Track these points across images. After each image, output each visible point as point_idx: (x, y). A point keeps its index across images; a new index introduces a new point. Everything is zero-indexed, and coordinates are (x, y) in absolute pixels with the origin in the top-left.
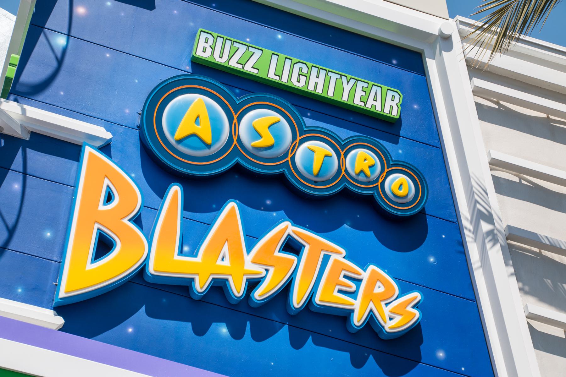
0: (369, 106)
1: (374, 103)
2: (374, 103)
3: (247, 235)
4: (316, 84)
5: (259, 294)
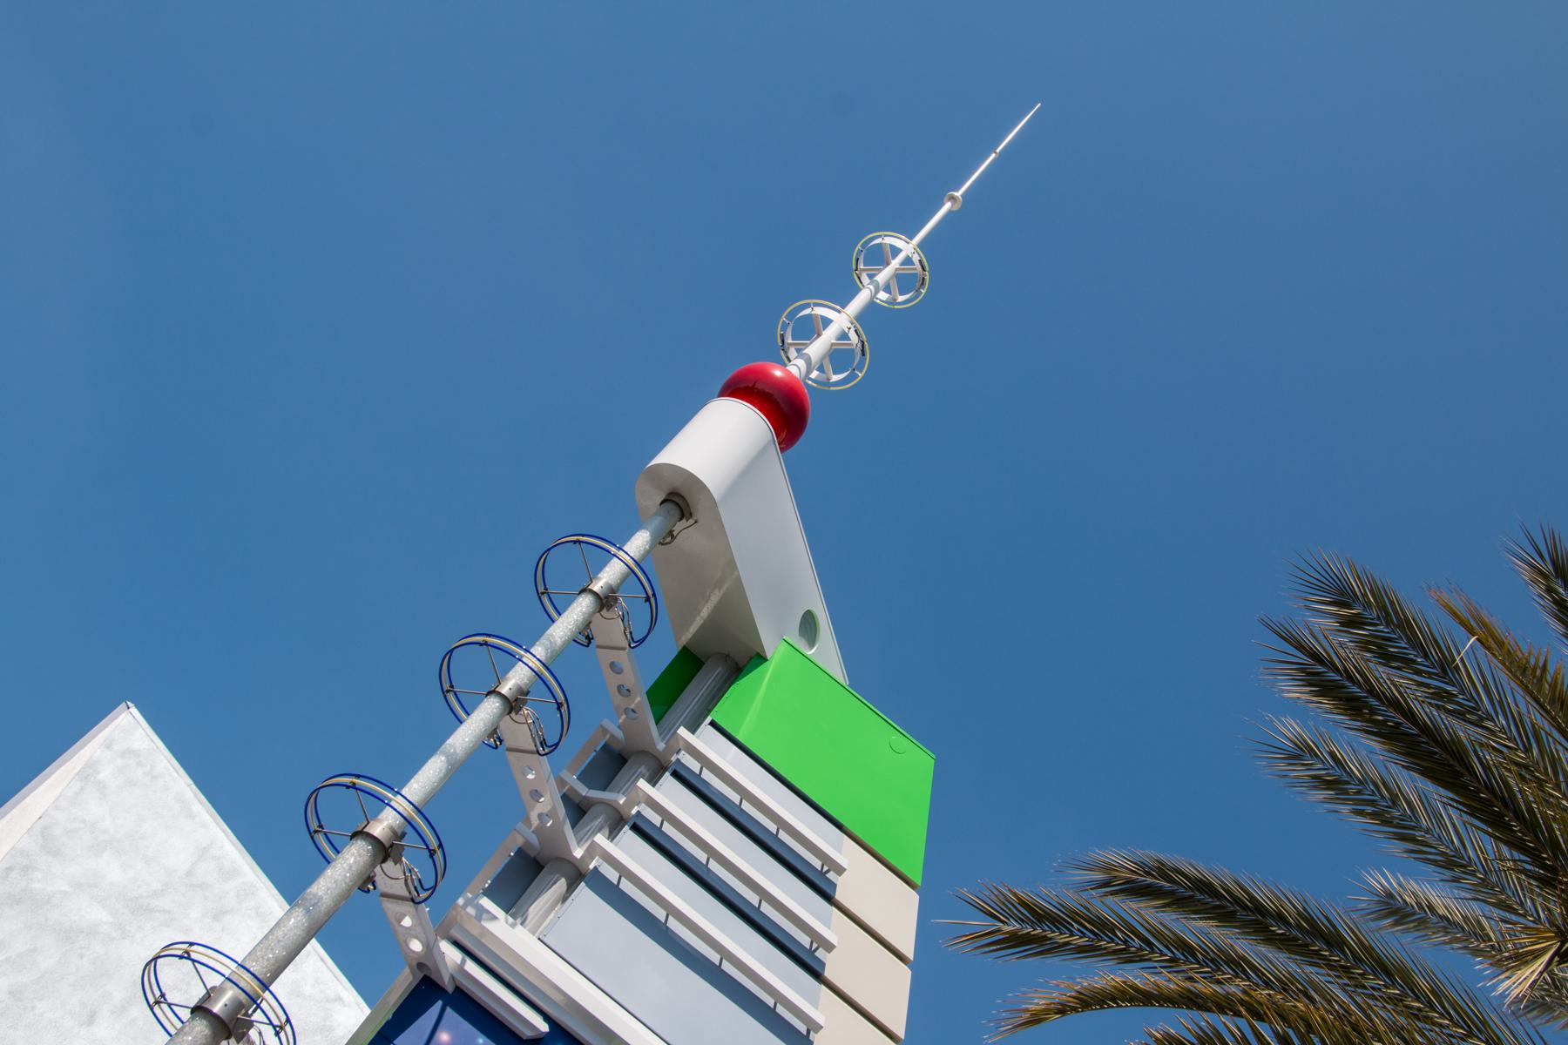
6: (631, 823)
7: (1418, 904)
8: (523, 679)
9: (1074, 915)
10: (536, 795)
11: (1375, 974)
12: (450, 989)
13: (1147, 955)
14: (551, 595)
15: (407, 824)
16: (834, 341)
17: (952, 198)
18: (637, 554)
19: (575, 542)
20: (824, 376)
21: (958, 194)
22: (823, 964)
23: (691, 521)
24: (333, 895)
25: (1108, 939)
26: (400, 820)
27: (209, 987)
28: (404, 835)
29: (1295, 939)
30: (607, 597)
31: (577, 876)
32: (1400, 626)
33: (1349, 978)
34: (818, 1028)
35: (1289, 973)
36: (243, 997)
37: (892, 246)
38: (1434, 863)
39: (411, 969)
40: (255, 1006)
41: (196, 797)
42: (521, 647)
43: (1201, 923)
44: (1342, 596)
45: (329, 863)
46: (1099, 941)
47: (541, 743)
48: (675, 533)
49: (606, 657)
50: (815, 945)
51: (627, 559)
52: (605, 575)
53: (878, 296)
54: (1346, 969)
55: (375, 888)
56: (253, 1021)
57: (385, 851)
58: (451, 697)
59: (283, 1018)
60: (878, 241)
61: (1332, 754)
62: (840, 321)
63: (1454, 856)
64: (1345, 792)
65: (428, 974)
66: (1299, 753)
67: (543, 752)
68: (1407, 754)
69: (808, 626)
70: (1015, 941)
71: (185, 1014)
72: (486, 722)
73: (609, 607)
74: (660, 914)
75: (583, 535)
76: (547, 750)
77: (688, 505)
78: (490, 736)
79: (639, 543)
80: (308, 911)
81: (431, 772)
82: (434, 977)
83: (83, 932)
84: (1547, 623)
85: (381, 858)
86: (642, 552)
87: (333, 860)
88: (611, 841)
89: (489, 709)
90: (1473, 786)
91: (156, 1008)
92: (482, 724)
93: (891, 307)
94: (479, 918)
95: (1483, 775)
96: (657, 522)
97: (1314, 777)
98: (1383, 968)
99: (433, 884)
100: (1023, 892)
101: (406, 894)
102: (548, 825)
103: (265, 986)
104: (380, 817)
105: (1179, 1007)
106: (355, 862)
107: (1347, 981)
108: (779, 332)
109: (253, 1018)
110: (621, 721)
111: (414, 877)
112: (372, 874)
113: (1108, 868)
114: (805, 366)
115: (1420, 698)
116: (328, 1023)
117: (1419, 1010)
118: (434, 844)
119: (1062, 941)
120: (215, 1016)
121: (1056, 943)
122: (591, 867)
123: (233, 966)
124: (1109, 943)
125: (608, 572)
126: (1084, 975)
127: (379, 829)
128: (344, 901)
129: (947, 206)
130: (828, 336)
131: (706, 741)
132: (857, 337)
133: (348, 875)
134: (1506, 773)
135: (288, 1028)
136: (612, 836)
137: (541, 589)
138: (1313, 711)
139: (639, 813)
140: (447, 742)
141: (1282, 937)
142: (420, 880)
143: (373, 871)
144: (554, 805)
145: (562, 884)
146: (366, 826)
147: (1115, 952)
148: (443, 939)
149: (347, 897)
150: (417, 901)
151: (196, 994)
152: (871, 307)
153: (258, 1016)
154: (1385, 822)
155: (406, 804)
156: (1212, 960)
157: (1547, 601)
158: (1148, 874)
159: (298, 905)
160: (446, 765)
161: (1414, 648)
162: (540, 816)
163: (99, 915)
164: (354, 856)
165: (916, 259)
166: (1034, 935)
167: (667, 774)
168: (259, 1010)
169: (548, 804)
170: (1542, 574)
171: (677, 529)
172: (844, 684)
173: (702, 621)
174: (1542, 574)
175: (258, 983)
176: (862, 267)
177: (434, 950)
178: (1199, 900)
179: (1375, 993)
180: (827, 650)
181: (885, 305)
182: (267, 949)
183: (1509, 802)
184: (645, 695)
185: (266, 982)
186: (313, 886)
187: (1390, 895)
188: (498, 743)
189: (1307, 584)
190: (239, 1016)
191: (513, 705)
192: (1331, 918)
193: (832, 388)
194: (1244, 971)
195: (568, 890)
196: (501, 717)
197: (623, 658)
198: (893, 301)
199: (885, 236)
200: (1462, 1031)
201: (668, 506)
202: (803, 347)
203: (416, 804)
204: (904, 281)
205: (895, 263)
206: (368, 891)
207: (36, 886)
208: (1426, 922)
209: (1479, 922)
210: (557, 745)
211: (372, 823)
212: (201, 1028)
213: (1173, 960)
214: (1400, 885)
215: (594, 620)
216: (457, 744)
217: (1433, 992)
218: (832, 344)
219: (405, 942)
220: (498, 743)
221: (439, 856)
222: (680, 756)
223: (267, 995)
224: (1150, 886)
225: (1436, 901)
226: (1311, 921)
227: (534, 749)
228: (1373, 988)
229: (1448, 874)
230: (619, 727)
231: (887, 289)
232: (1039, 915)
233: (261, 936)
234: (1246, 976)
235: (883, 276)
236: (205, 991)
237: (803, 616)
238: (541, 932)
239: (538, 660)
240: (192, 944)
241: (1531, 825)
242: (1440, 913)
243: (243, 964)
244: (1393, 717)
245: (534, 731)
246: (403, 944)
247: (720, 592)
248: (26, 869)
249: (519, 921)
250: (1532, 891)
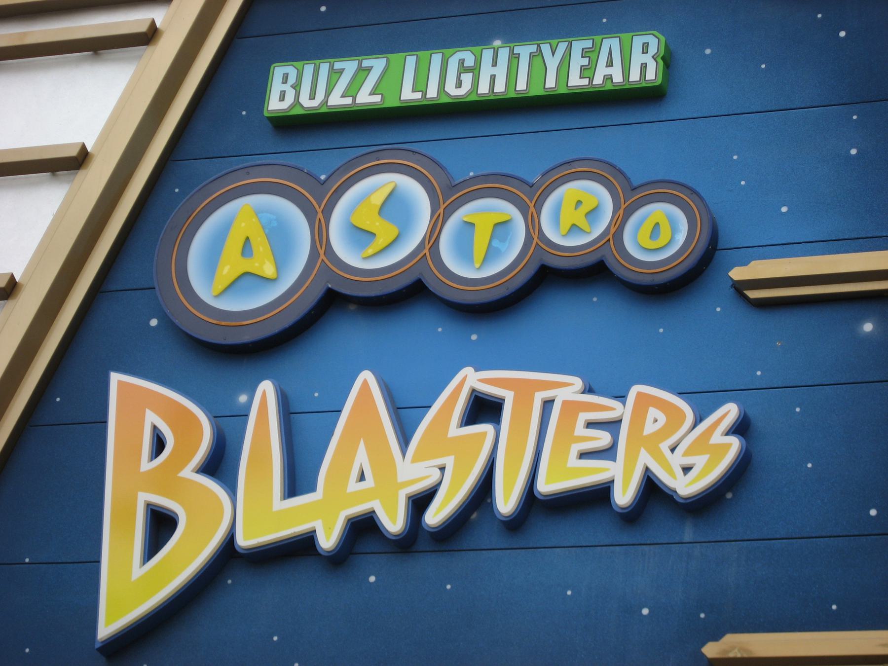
0: (598, 80)
1: (609, 71)
2: (609, 71)
3: (215, 417)
4: (493, 78)
5: (434, 516)
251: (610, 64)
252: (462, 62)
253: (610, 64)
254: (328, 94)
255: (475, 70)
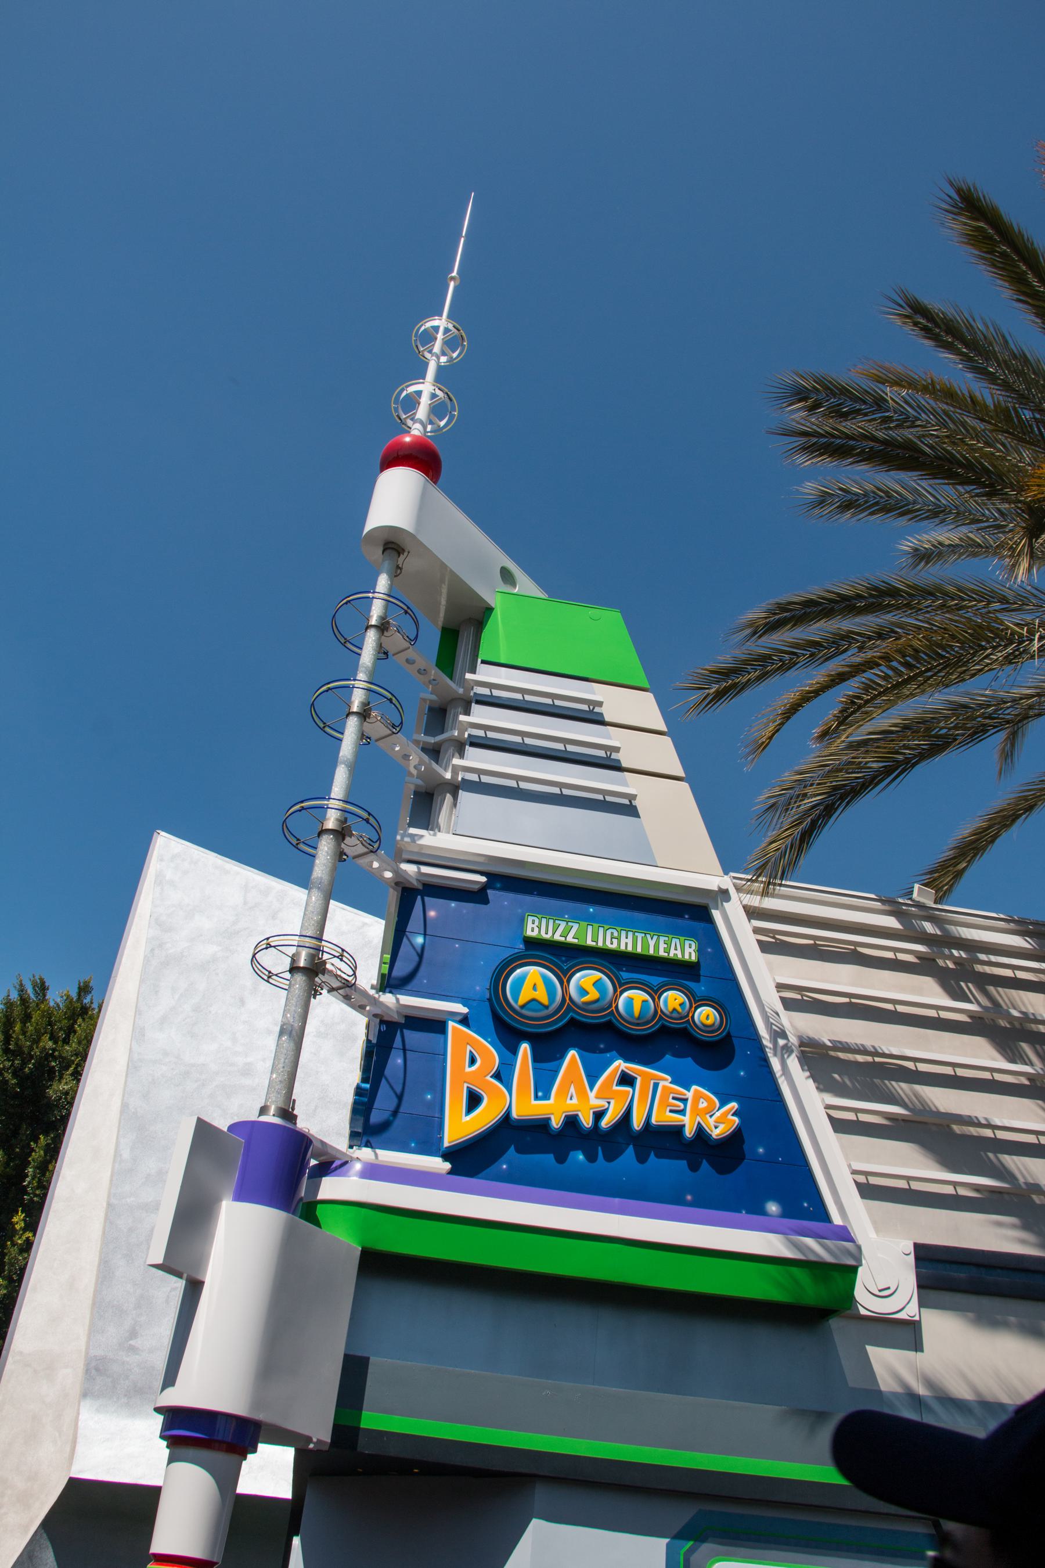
0: (671, 955)
1: (676, 952)
2: (676, 952)
4: (626, 944)
5: (605, 1123)
6: (468, 743)
7: (933, 545)
8: (361, 697)
9: (746, 662)
10: (406, 757)
11: (924, 599)
12: (420, 887)
13: (796, 660)
14: (350, 641)
15: (344, 812)
16: (429, 402)
17: (452, 278)
18: (386, 590)
19: (346, 603)
20: (436, 426)
21: (454, 274)
22: (619, 761)
23: (406, 554)
24: (328, 872)
25: (770, 664)
26: (339, 813)
27: (291, 956)
28: (346, 820)
29: (873, 604)
30: (382, 624)
31: (454, 788)
32: (842, 393)
33: (911, 609)
34: (634, 797)
35: (878, 625)
36: (312, 951)
37: (433, 327)
38: (927, 518)
39: (394, 889)
40: (321, 952)
41: (224, 861)
42: (350, 680)
43: (818, 625)
44: (800, 394)
45: (314, 857)
46: (766, 668)
47: (393, 727)
48: (400, 566)
49: (401, 659)
50: (608, 753)
51: (381, 596)
52: (374, 612)
53: (441, 361)
54: (908, 606)
55: (348, 856)
56: (325, 960)
57: (341, 834)
58: (327, 729)
59: (340, 951)
60: (423, 328)
61: (841, 489)
62: (426, 388)
63: (935, 509)
64: (860, 505)
65: (404, 886)
66: (823, 499)
67: (397, 732)
68: (884, 463)
69: (507, 576)
70: (719, 695)
71: (288, 975)
72: (355, 732)
73: (387, 629)
74: (512, 783)
75: (349, 597)
76: (398, 729)
77: (398, 545)
78: (362, 739)
79: (383, 583)
80: (319, 888)
81: (341, 777)
82: (407, 885)
83: (210, 962)
84: (923, 344)
85: (341, 838)
86: (388, 587)
87: (317, 853)
88: (463, 759)
89: (352, 725)
90: (928, 461)
91: (270, 980)
92: (353, 735)
93: (452, 363)
94: (414, 841)
95: (931, 452)
96: (386, 564)
97: (838, 507)
98: (928, 593)
99: (378, 837)
100: (710, 666)
101: (366, 850)
102: (423, 769)
103: (320, 939)
104: (327, 817)
105: (834, 687)
106: (328, 849)
107: (910, 612)
108: (395, 415)
109: (324, 959)
110: (430, 689)
111: (365, 839)
112: (342, 850)
113: (751, 624)
114: (420, 425)
115: (878, 428)
116: (367, 940)
117: (956, 605)
118: (365, 815)
119: (746, 680)
120: (303, 968)
121: (743, 683)
122: (460, 779)
123: (297, 938)
124: (772, 666)
125: (375, 610)
126: (773, 700)
127: (331, 824)
128: (334, 871)
129: (452, 285)
130: (425, 401)
131: (484, 674)
132: (442, 392)
133: (328, 857)
134: (944, 446)
135: (345, 954)
136: (462, 756)
137: (343, 641)
138: (822, 467)
139: (469, 735)
140: (340, 755)
141: (866, 606)
142: (369, 839)
143: (341, 848)
144: (420, 758)
145: (449, 797)
146: (323, 826)
147: (779, 668)
148: (401, 863)
149: (336, 870)
150: (375, 850)
151: (287, 962)
152: (440, 370)
153: (326, 956)
154: (889, 511)
155: (337, 802)
156: (833, 643)
157: (917, 331)
158: (775, 614)
159: (311, 888)
160: (346, 769)
161: (856, 402)
162: (415, 767)
163: (212, 949)
164: (326, 847)
165: (450, 326)
166: (729, 686)
167: (473, 704)
168: (324, 953)
169: (416, 758)
170: (906, 317)
171: (400, 563)
172: (546, 598)
173: (445, 607)
174: (906, 317)
175: (315, 940)
176: (422, 349)
177: (399, 871)
178: (810, 612)
179: (928, 609)
180: (525, 584)
181: (448, 364)
182: (309, 919)
183: (951, 460)
184: (436, 668)
185: (319, 937)
186: (313, 873)
187: (916, 550)
188: (369, 740)
189: (776, 399)
190: (316, 962)
191: (364, 715)
192: (886, 580)
193: (444, 430)
194: (853, 639)
195: (454, 799)
196: (361, 725)
197: (411, 653)
198: (451, 359)
199: (425, 323)
200: (984, 603)
201: (388, 551)
202: (414, 416)
203: (343, 799)
204: (450, 344)
205: (440, 336)
206: (345, 860)
207: (171, 951)
208: (942, 553)
209: (968, 537)
210: (402, 723)
211: (324, 822)
212: (300, 979)
213: (812, 655)
214: (919, 541)
215: (382, 641)
216: (347, 754)
217: (959, 590)
218: (430, 405)
219: (381, 875)
220: (369, 740)
221: (372, 820)
222: (475, 691)
223: (324, 943)
224: (779, 620)
225: (940, 538)
226: (876, 589)
227: (390, 732)
228: (927, 607)
229: (937, 520)
230: (431, 693)
231: (444, 354)
232: (726, 673)
233: (302, 914)
234: (856, 640)
235: (437, 348)
236: (290, 959)
237: (500, 572)
238: (453, 829)
239: (364, 681)
240: (268, 939)
241: (969, 466)
242: (946, 544)
243: (301, 934)
244: (867, 445)
245: (384, 722)
246: (380, 877)
247: (445, 585)
248: (161, 946)
249: (436, 830)
250: (985, 504)
251: (676, 949)
252: (612, 933)
253: (676, 949)
254: (553, 934)
255: (619, 939)
